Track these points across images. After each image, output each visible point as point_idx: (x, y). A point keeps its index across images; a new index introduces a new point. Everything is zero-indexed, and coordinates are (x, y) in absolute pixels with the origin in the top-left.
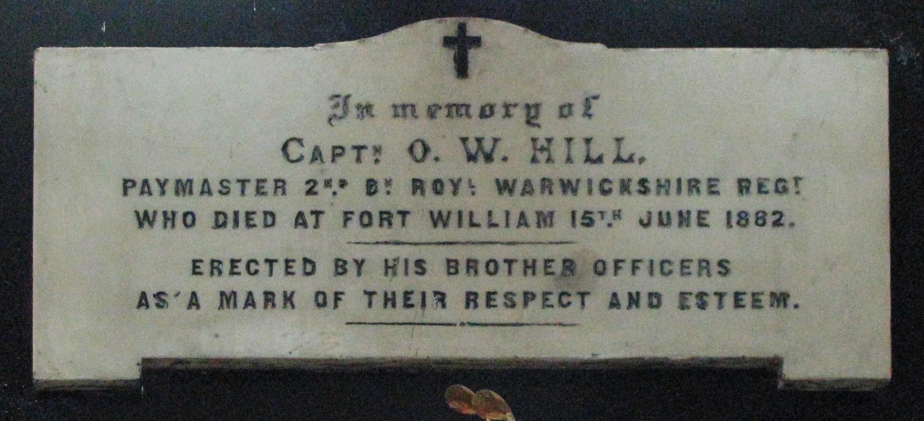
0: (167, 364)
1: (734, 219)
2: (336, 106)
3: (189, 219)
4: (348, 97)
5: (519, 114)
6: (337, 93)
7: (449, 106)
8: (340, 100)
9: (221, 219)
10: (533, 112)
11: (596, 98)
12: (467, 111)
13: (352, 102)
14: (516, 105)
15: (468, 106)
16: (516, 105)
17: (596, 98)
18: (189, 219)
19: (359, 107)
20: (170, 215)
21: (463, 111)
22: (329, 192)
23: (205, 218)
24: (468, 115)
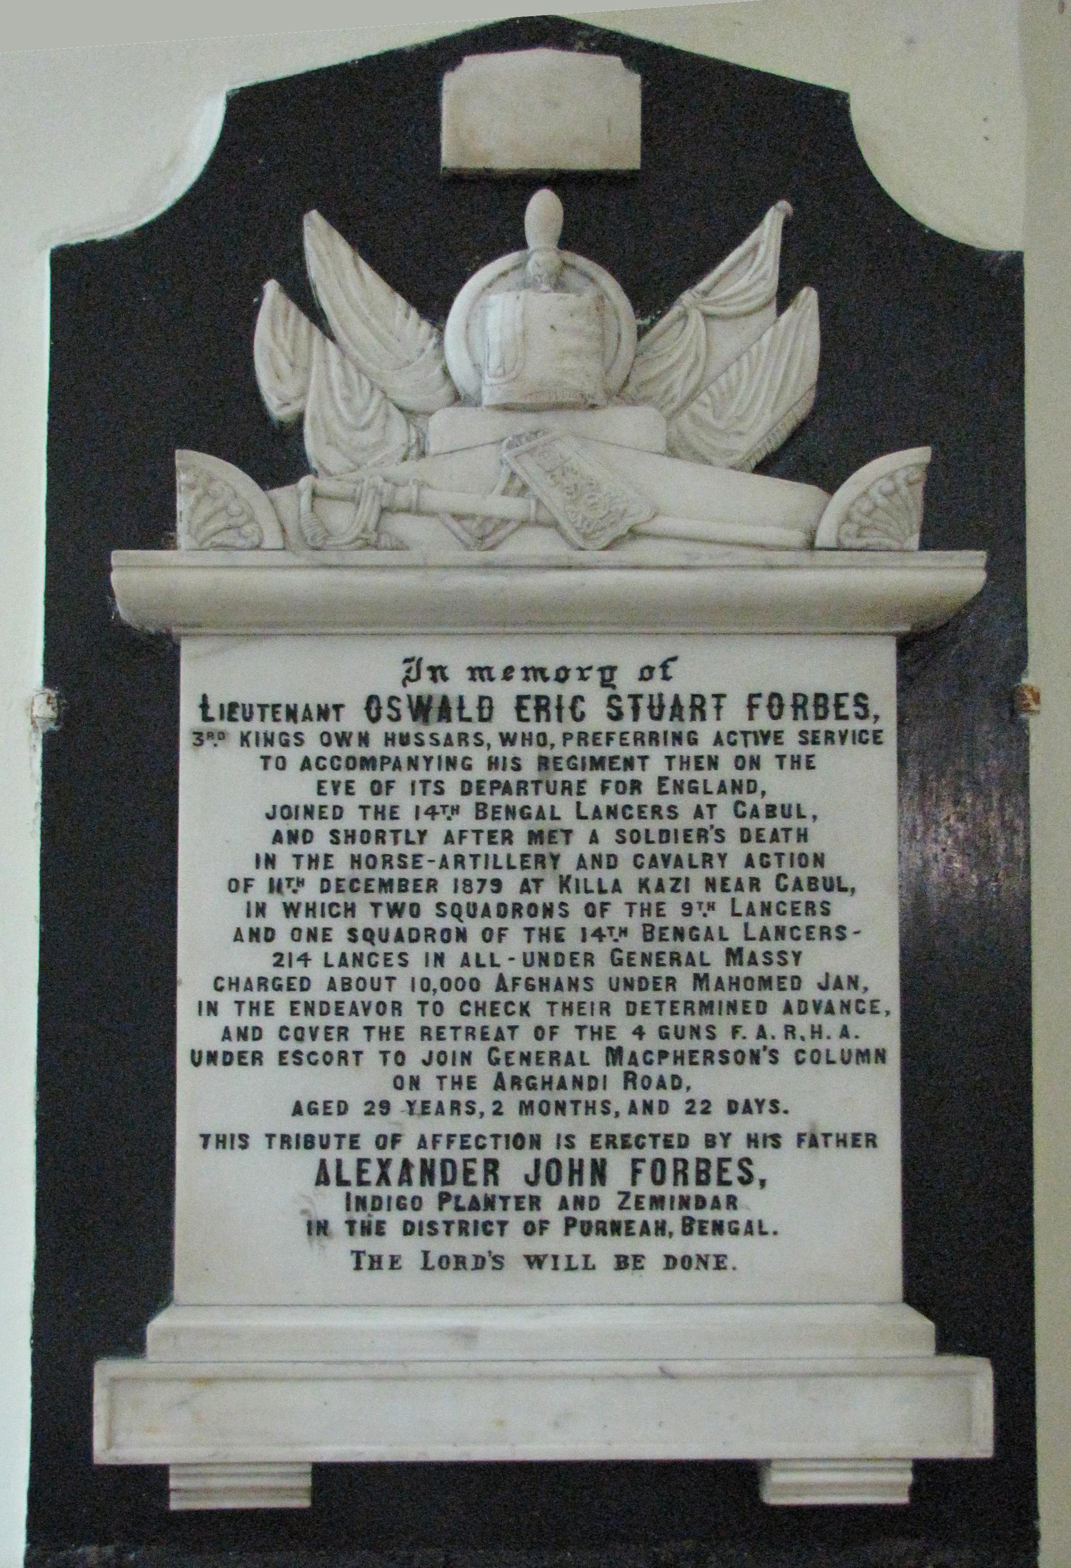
0: (548, 175)
1: (460, 886)
2: (409, 671)
3: (529, 1229)
4: (421, 659)
5: (595, 676)
6: (409, 656)
7: (525, 669)
8: (414, 664)
9: (409, 1227)
10: (607, 676)
11: (674, 659)
12: (489, 674)
13: (424, 665)
14: (590, 668)
15: (489, 669)
16: (590, 668)
17: (674, 659)
18: (529, 1229)
19: (432, 669)
20: (376, 1265)
21: (485, 674)
22: (813, 829)
23: (719, 1108)
24: (492, 679)
